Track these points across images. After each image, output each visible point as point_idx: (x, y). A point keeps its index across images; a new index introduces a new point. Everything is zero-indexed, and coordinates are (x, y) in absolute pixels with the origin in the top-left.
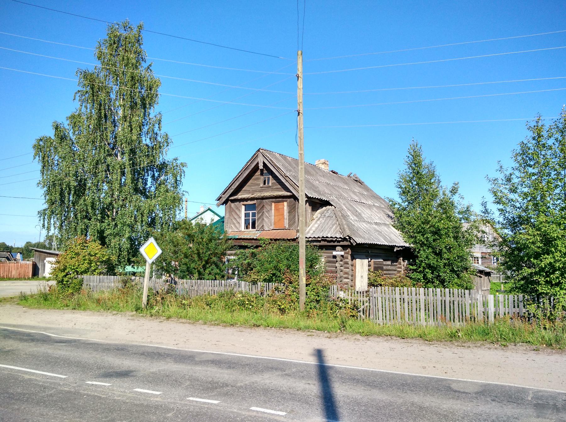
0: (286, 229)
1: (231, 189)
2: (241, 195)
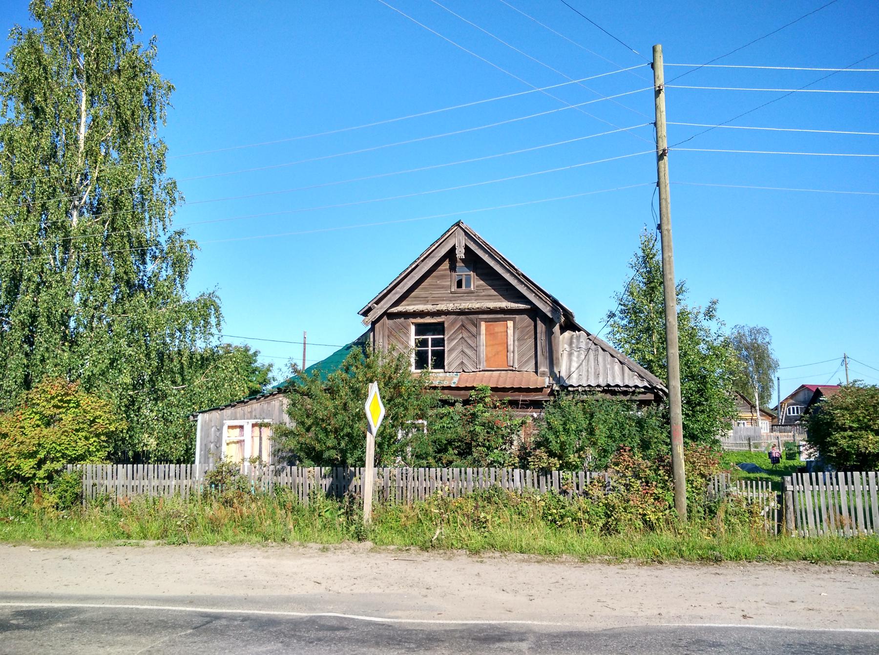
0: (513, 370)
1: (396, 293)
2: (408, 305)
